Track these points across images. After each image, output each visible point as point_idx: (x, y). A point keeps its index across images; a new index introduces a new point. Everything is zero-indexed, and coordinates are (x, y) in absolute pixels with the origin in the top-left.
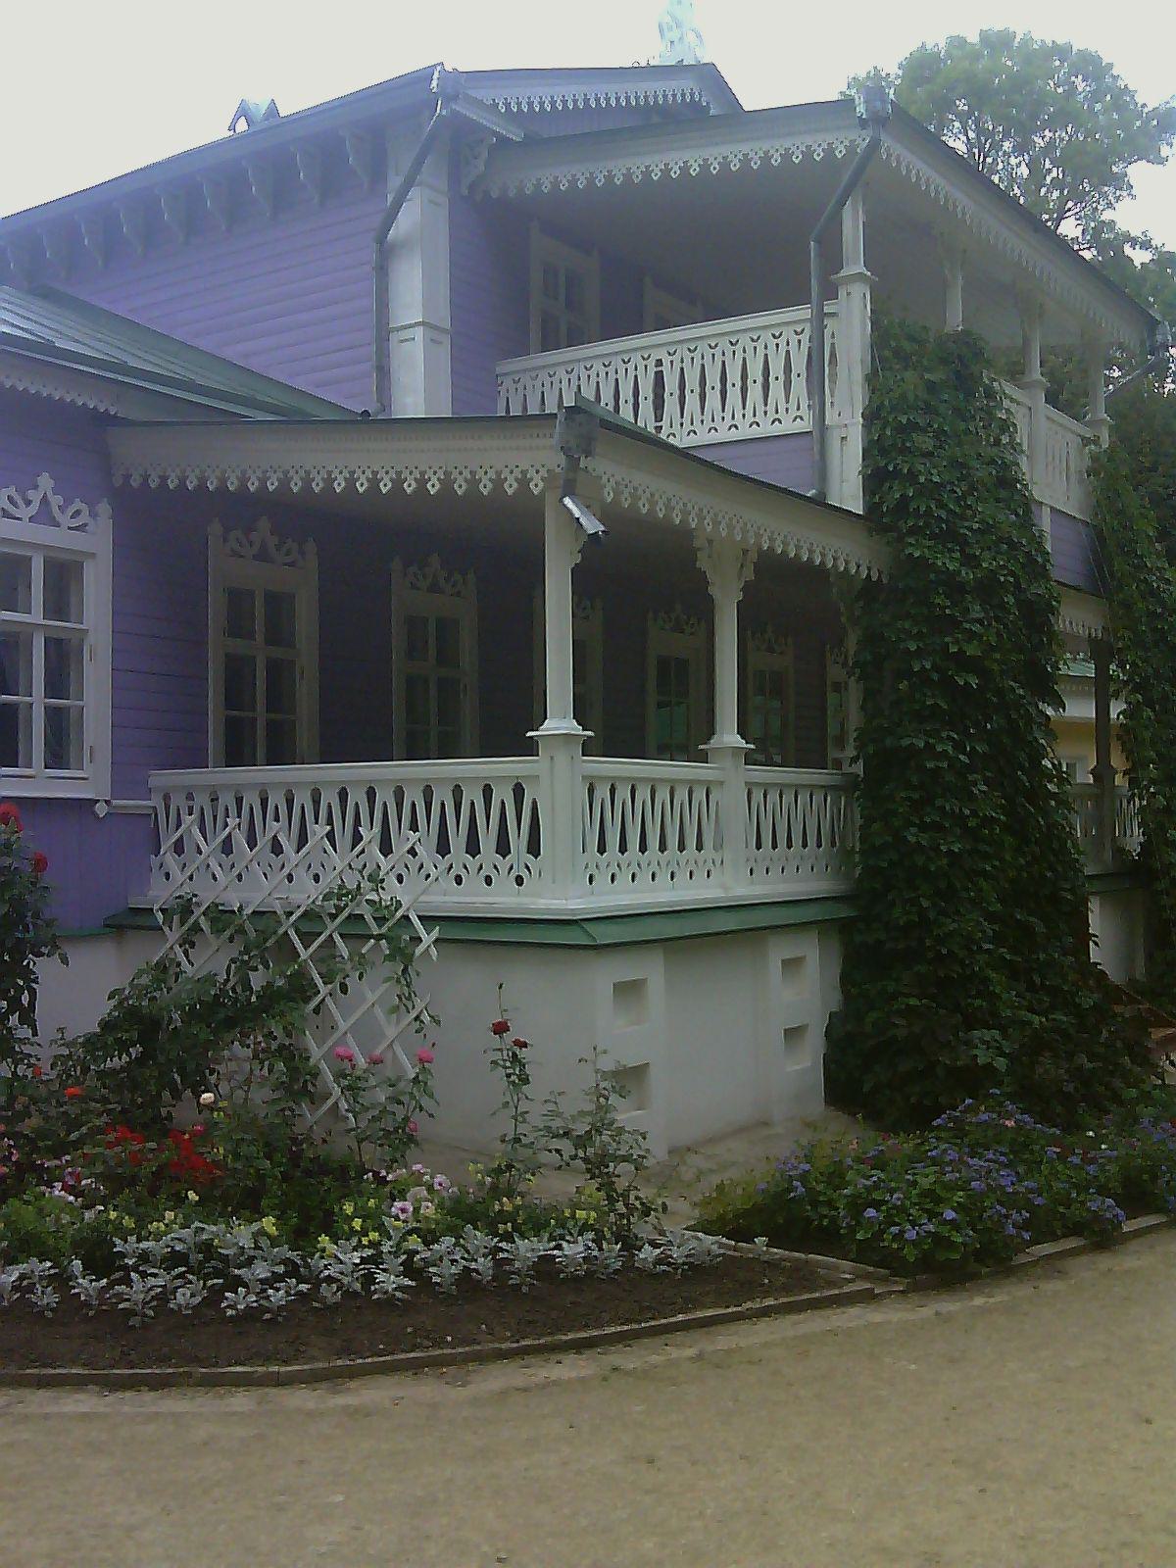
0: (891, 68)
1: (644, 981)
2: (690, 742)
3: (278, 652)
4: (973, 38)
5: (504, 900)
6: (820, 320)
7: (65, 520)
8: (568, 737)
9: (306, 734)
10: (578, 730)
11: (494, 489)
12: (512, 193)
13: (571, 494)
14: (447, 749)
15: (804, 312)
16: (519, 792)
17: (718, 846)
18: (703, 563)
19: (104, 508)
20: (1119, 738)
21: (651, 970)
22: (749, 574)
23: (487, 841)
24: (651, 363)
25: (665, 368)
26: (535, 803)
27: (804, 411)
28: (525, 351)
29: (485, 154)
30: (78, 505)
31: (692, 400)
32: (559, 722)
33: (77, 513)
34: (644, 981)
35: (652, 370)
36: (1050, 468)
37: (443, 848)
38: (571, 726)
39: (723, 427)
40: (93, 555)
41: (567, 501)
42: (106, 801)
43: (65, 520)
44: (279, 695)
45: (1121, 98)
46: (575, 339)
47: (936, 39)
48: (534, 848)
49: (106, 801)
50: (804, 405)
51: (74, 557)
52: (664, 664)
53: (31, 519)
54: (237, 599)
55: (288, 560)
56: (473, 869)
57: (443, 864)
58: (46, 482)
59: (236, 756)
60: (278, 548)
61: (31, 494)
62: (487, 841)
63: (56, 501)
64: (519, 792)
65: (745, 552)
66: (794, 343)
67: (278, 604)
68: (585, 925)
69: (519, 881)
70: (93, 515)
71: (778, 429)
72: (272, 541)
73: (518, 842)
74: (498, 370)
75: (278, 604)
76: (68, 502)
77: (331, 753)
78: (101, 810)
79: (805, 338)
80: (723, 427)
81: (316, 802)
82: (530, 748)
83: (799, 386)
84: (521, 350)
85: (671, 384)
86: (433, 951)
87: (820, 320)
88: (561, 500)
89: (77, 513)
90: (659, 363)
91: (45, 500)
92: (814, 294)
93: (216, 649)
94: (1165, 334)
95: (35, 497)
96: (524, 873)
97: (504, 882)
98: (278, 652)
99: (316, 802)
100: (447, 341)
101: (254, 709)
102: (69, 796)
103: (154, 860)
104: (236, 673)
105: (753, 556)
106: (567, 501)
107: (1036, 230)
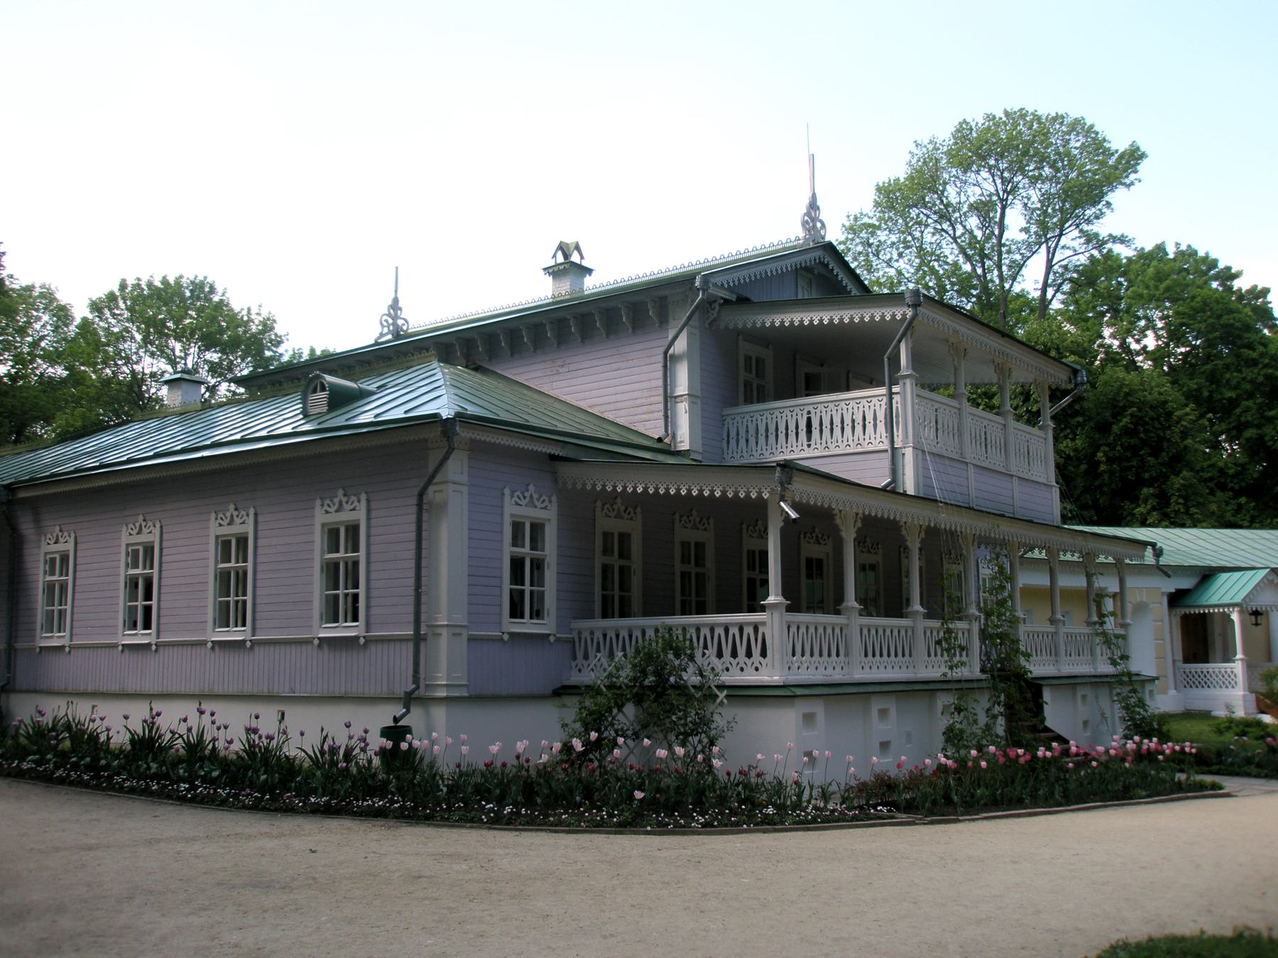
1: (815, 714)
2: (835, 606)
3: (624, 562)
4: (999, 114)
5: (750, 678)
6: (891, 395)
9: (804, 605)
10: (784, 601)
11: (745, 496)
13: (785, 501)
14: (701, 610)
15: (883, 390)
16: (756, 629)
17: (847, 655)
18: (838, 521)
20: (1094, 601)
21: (818, 708)
22: (859, 524)
23: (742, 651)
24: (805, 412)
25: (812, 415)
26: (764, 634)
27: (884, 439)
28: (736, 404)
29: (717, 308)
30: (544, 497)
31: (826, 432)
33: (544, 501)
34: (815, 714)
35: (805, 416)
36: (1018, 455)
37: (720, 655)
38: (780, 599)
39: (842, 446)
40: (549, 520)
41: (782, 504)
42: (554, 635)
44: (624, 586)
45: (1097, 145)
46: (762, 399)
47: (976, 118)
49: (554, 635)
50: (884, 437)
51: (540, 521)
52: (809, 561)
53: (526, 505)
54: (607, 536)
55: (543, 505)
56: (734, 665)
57: (749, 662)
58: (531, 488)
59: (605, 615)
60: (625, 511)
61: (527, 494)
62: (742, 651)
63: (536, 496)
64: (756, 629)
65: (857, 514)
66: (878, 406)
67: (624, 538)
68: (792, 689)
69: (742, 669)
70: (550, 502)
72: (536, 496)
73: (756, 651)
74: (724, 413)
75: (624, 538)
77: (646, 613)
79: (883, 403)
80: (842, 446)
83: (881, 427)
84: (735, 404)
85: (815, 424)
86: (725, 701)
87: (891, 395)
88: (779, 503)
89: (544, 501)
90: (809, 412)
91: (531, 496)
92: (887, 380)
93: (599, 560)
94: (1082, 377)
96: (744, 666)
98: (624, 562)
100: (699, 401)
101: (613, 590)
102: (519, 631)
103: (574, 664)
104: (606, 570)
105: (861, 515)
106: (782, 504)
107: (1003, 336)
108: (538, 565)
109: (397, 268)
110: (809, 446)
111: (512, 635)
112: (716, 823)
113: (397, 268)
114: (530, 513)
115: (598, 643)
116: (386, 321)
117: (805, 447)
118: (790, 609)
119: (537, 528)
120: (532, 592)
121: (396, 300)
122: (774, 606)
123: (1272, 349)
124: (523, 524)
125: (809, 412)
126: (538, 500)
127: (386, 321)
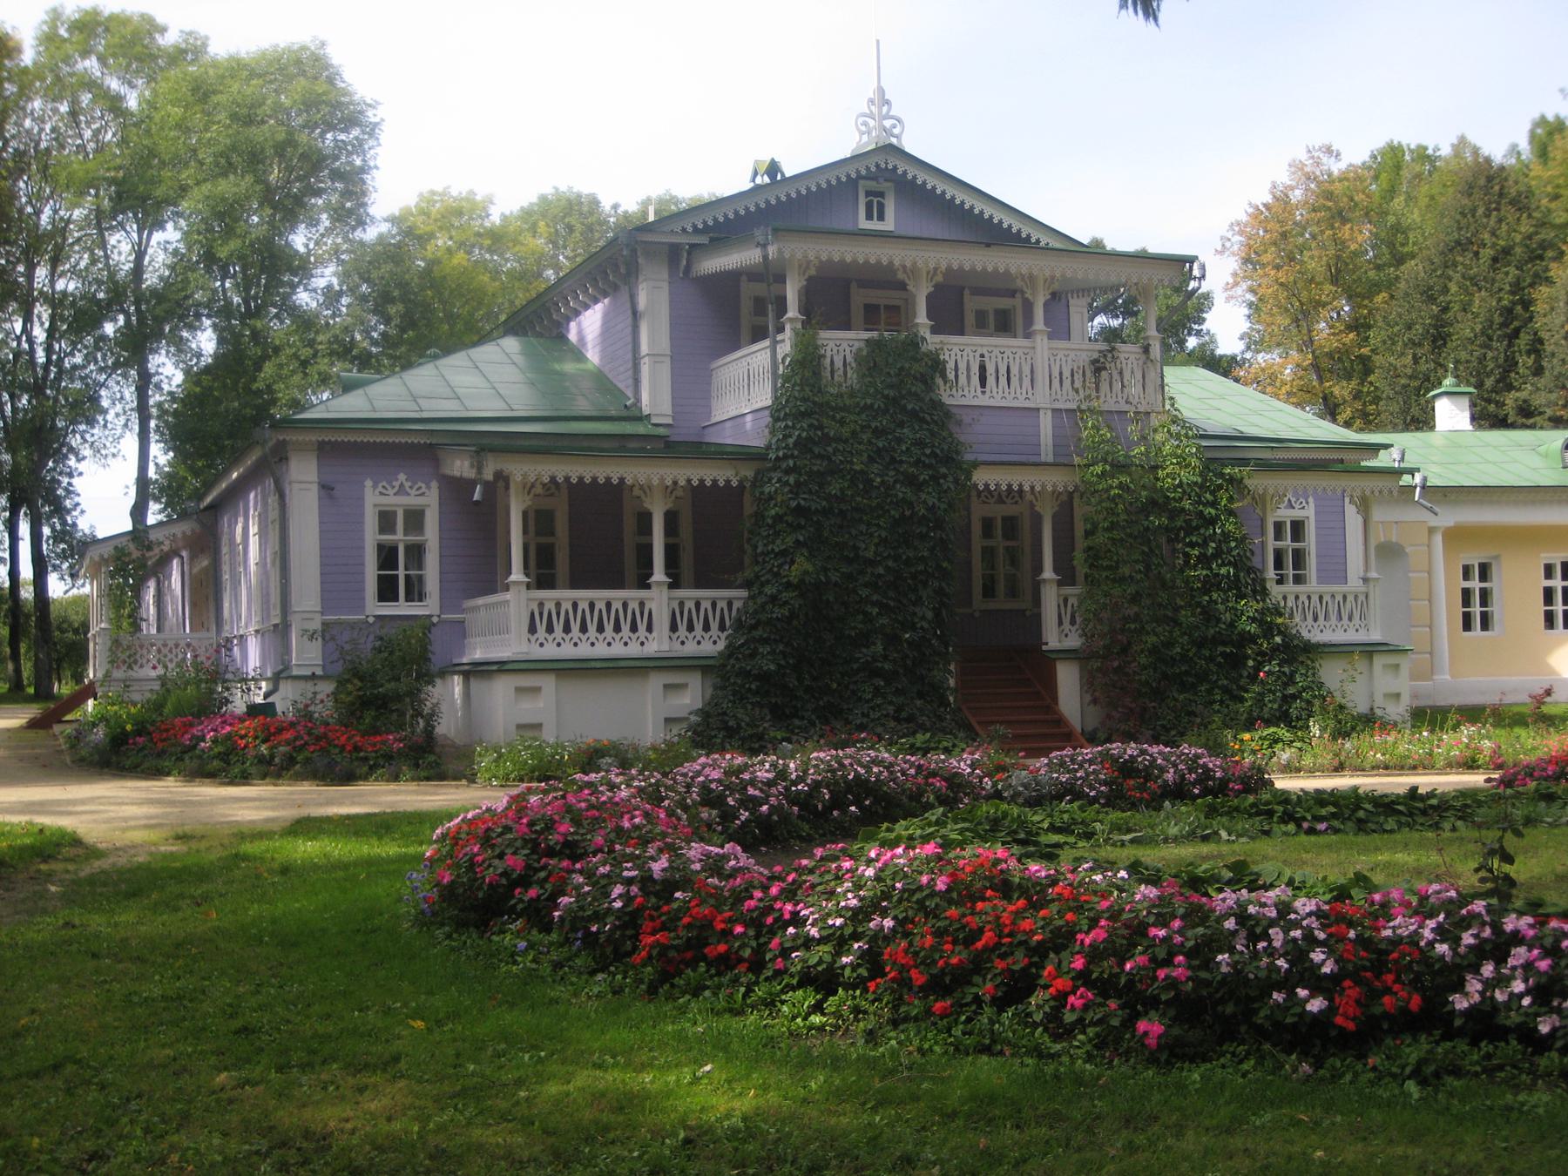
0: (107, 13)
7: (413, 492)
8: (664, 582)
12: (990, 269)
16: (642, 604)
19: (434, 484)
21: (548, 683)
24: (978, 355)
30: (420, 484)
32: (517, 575)
43: (1297, 506)
48: (650, 629)
58: (402, 477)
63: (407, 484)
64: (642, 604)
70: (429, 487)
71: (1015, 404)
73: (642, 627)
76: (415, 483)
77: (575, 584)
78: (1028, 613)
81: (698, 610)
82: (648, 587)
89: (419, 488)
95: (396, 484)
97: (1351, 632)
99: (698, 610)
108: (416, 553)
109: (878, 42)
110: (982, 356)
111: (378, 617)
112: (1278, 639)
113: (878, 42)
114: (398, 502)
115: (634, 613)
116: (865, 124)
117: (987, 355)
118: (672, 586)
119: (415, 519)
120: (407, 577)
121: (881, 91)
122: (659, 583)
123: (1560, 218)
124: (395, 513)
125: (982, 356)
126: (411, 487)
127: (865, 124)
